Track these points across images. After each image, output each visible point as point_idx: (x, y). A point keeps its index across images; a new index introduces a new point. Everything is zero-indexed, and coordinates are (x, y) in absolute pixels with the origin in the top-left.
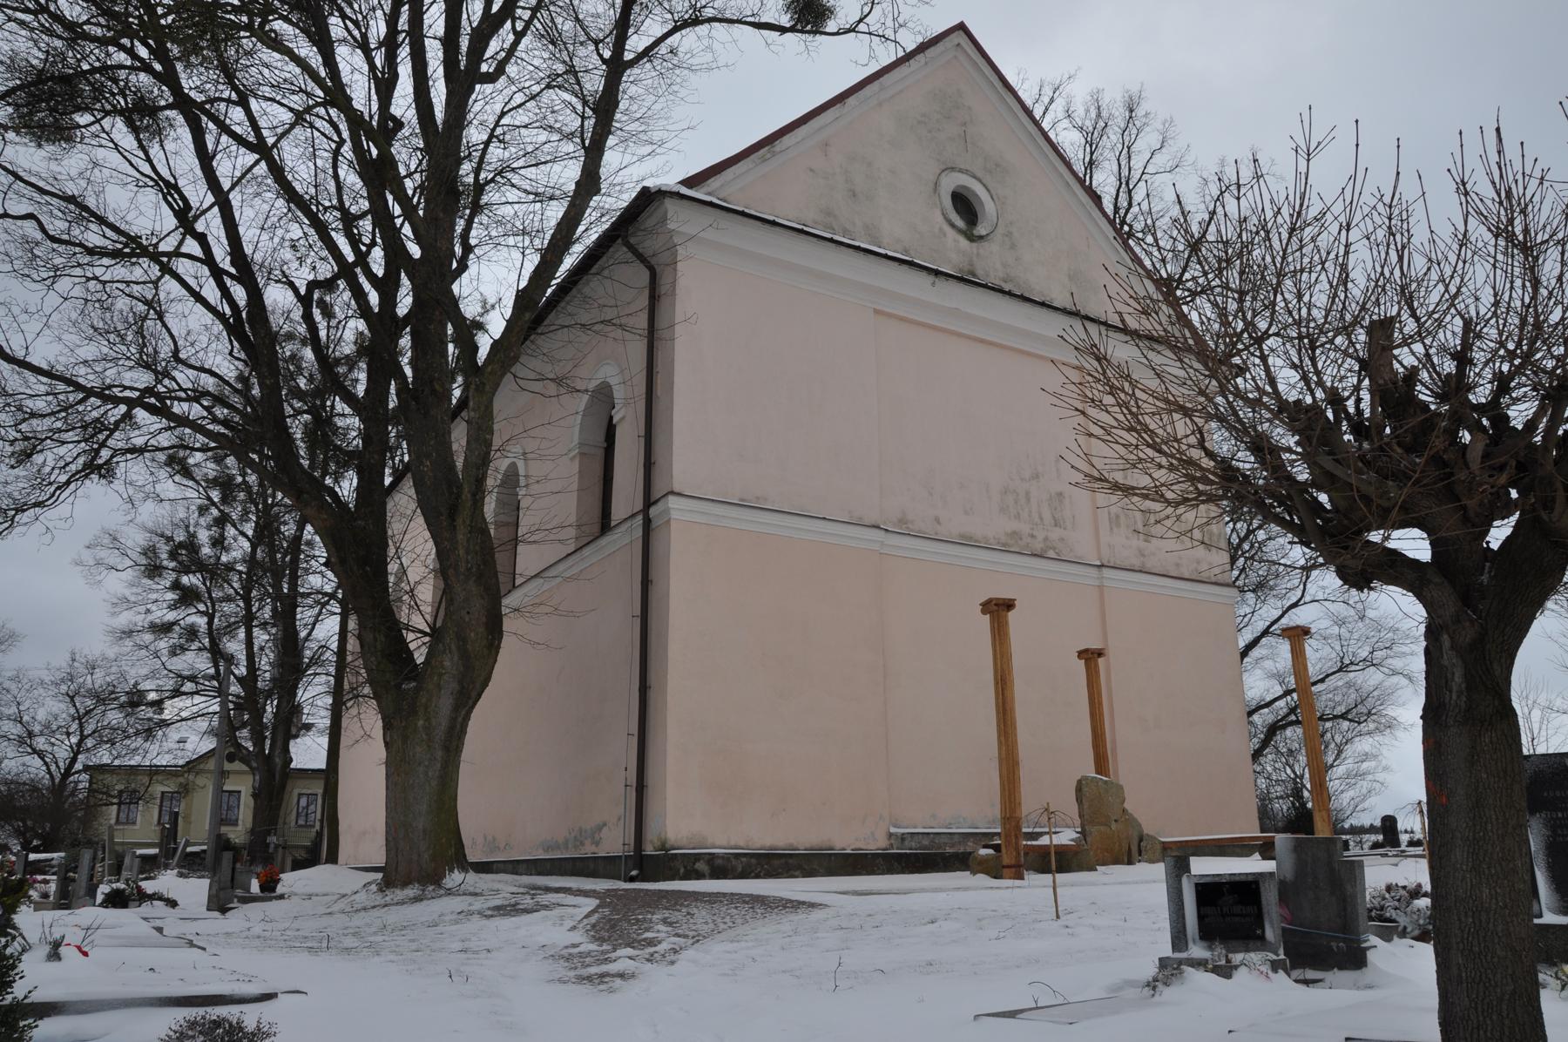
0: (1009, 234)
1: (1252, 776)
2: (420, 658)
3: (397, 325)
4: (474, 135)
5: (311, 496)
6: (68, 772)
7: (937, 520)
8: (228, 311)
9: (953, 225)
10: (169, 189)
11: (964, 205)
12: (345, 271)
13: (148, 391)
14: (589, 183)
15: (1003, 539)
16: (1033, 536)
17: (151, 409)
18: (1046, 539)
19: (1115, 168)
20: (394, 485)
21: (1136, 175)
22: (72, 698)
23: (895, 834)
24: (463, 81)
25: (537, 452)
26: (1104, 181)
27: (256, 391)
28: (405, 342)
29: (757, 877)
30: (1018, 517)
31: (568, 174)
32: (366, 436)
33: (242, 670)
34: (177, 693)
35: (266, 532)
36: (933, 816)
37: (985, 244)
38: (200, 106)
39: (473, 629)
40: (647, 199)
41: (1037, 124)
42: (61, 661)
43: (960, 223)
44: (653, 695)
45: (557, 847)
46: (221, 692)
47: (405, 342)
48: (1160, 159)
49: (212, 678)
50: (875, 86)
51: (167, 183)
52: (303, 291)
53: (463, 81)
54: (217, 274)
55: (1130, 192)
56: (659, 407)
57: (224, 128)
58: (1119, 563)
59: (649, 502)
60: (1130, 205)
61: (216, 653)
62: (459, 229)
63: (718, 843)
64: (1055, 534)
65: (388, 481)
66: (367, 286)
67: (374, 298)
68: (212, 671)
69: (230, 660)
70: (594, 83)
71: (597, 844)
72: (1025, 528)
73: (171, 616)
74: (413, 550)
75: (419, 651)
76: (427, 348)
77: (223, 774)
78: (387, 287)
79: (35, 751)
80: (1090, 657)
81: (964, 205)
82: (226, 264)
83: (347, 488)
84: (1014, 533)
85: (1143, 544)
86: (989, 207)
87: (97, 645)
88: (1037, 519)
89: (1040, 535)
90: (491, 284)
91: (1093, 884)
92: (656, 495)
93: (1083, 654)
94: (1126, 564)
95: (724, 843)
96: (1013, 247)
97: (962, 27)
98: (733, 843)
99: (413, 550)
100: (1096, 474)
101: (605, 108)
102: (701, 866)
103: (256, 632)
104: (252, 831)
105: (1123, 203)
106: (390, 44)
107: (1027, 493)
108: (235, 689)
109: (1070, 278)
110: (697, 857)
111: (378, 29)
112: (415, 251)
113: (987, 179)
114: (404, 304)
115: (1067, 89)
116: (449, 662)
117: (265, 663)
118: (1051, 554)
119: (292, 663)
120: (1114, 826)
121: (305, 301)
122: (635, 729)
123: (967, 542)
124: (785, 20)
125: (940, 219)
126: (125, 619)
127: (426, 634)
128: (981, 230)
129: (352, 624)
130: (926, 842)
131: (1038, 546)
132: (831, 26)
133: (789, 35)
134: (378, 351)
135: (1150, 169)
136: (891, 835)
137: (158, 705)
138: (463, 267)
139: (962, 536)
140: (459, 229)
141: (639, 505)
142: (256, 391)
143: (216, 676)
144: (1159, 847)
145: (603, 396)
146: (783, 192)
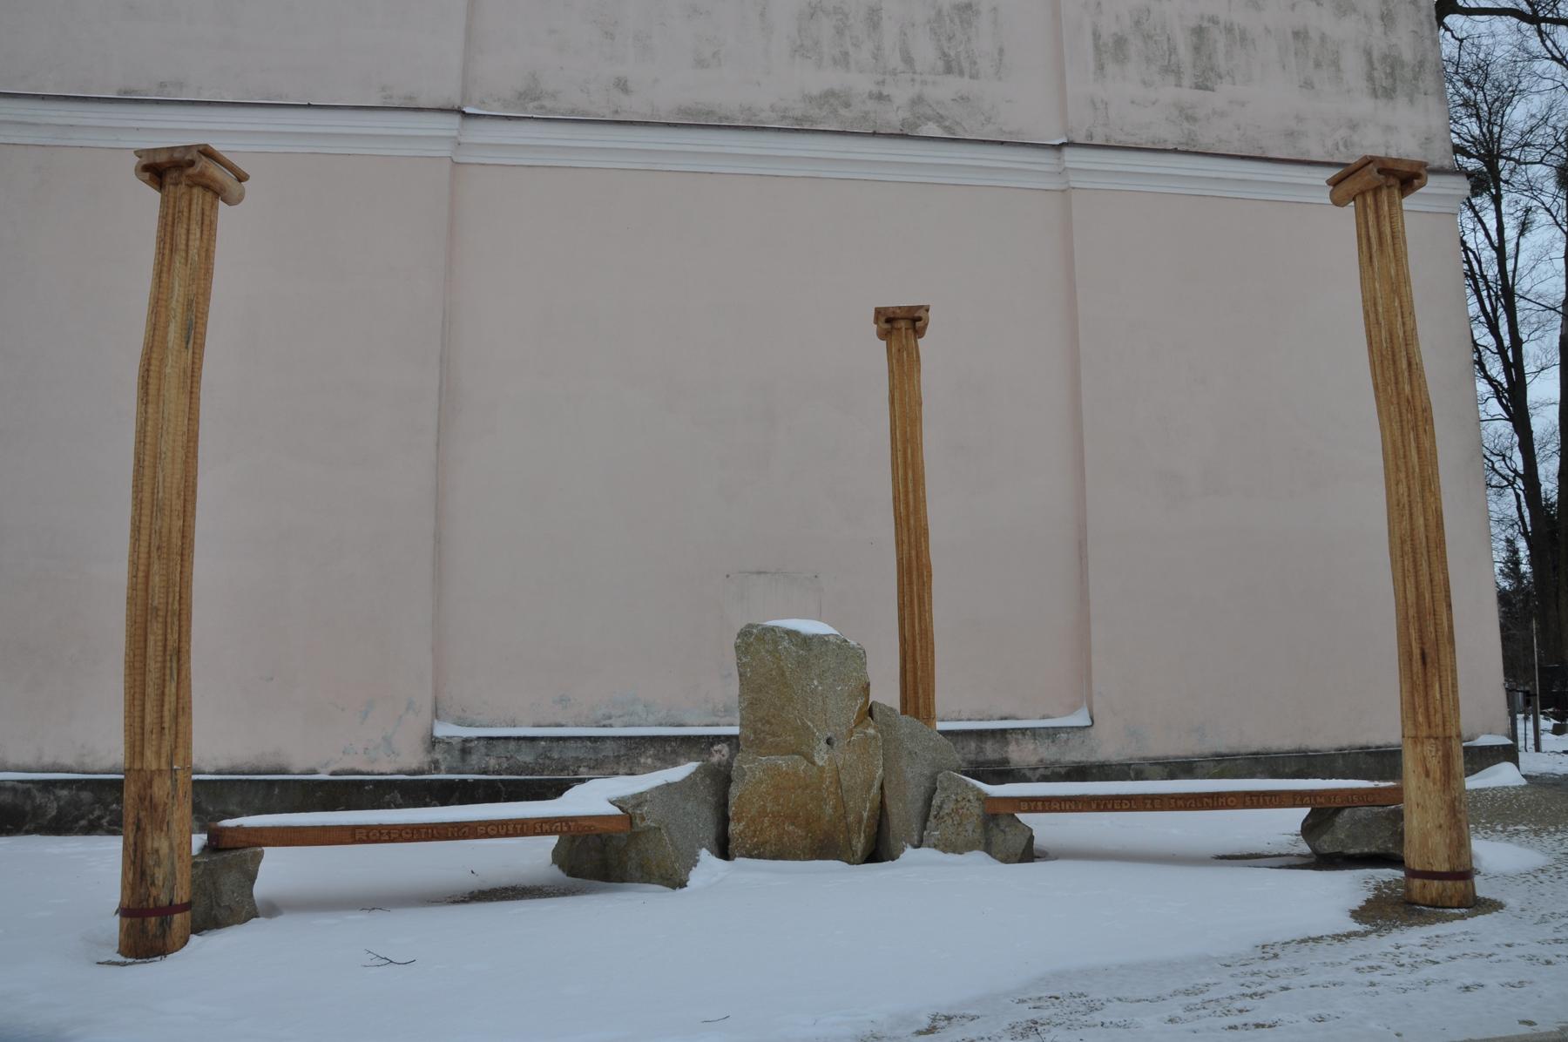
7: (622, 86)
16: (880, 97)
18: (918, 101)
23: (448, 742)
30: (843, 60)
58: (1119, 138)
64: (944, 90)
72: (861, 83)
80: (901, 325)
84: (830, 94)
85: (1188, 95)
88: (895, 61)
89: (901, 94)
93: (161, 170)
95: (28, 758)
98: (47, 760)
100: (1510, 248)
118: (931, 129)
120: (821, 757)
130: (526, 756)
131: (894, 118)
136: (434, 742)
144: (976, 809)
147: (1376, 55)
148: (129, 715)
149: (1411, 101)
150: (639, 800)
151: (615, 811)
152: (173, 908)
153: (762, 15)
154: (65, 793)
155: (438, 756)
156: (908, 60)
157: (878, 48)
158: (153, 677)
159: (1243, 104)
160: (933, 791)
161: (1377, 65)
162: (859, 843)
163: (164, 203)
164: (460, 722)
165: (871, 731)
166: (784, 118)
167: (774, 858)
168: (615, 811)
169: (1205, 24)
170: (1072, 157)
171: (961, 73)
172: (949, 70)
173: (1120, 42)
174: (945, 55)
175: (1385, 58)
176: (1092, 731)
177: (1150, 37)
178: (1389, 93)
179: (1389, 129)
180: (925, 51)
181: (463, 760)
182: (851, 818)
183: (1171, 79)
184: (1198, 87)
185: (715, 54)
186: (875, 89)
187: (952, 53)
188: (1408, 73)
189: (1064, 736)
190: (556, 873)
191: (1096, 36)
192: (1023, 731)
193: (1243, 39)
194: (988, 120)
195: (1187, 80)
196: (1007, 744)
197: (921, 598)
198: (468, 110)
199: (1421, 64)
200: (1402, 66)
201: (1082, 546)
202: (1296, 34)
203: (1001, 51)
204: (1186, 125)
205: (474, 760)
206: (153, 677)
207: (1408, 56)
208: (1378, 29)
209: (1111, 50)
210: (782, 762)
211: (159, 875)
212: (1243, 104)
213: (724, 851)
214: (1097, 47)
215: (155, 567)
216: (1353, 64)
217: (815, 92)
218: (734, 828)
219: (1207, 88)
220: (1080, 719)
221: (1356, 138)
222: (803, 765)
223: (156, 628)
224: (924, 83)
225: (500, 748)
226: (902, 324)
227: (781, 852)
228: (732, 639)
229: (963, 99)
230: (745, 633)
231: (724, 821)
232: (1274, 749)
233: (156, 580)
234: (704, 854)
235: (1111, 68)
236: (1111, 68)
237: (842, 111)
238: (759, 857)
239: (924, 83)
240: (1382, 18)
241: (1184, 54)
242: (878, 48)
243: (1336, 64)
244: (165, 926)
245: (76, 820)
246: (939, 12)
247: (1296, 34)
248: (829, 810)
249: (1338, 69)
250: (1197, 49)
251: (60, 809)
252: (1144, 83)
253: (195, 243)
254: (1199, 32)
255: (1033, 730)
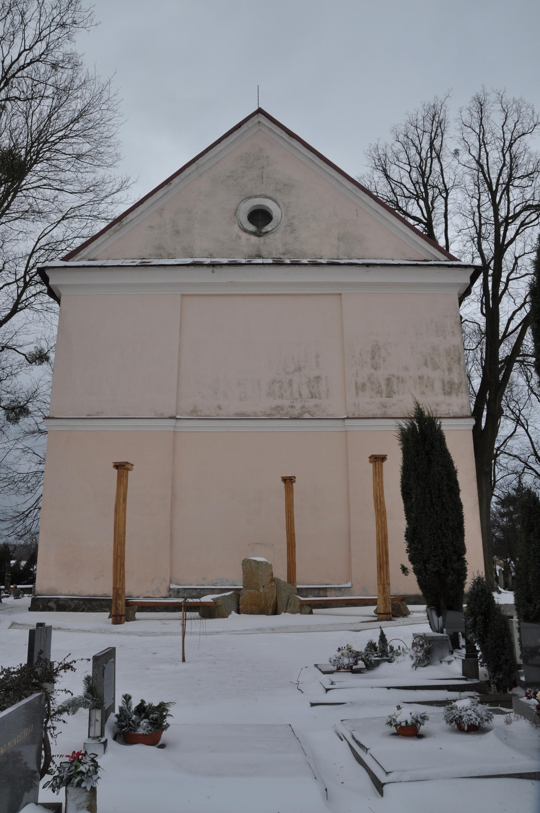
1: (79, 790)
7: (219, 407)
15: (269, 412)
16: (292, 407)
18: (303, 407)
19: (395, 179)
27: (493, 461)
29: (83, 611)
30: (281, 396)
36: (204, 579)
37: (271, 236)
50: (193, 167)
58: (363, 415)
63: (63, 593)
64: (311, 403)
72: (286, 403)
84: (277, 407)
85: (384, 399)
88: (296, 395)
89: (298, 405)
91: (308, 629)
94: (370, 414)
95: (67, 593)
96: (293, 231)
97: (260, 111)
98: (71, 593)
102: (51, 604)
110: (50, 600)
118: (307, 416)
120: (261, 590)
123: (242, 417)
131: (296, 413)
136: (170, 589)
139: (237, 414)
142: (493, 461)
144: (298, 603)
147: (446, 382)
148: (114, 577)
149: (457, 395)
150: (218, 599)
151: (212, 601)
152: (122, 615)
153: (258, 384)
154: (76, 601)
155: (171, 593)
156: (300, 395)
157: (292, 392)
158: (119, 569)
159: (402, 401)
160: (289, 599)
161: (446, 385)
162: (270, 611)
163: (118, 472)
164: (177, 584)
165: (273, 584)
166: (264, 414)
167: (250, 614)
168: (212, 601)
169: (390, 377)
170: (347, 422)
171: (316, 398)
172: (312, 397)
173: (364, 385)
174: (311, 392)
175: (448, 382)
176: (352, 589)
177: (373, 383)
178: (450, 393)
179: (449, 405)
180: (306, 392)
181: (178, 594)
182: (268, 605)
183: (379, 395)
184: (388, 397)
185: (245, 397)
186: (291, 405)
187: (313, 392)
188: (456, 386)
189: (343, 590)
190: (200, 617)
191: (356, 384)
192: (331, 588)
193: (402, 380)
194: (324, 411)
195: (384, 395)
196: (327, 592)
197: (292, 552)
198: (178, 417)
199: (461, 383)
200: (455, 384)
201: (350, 534)
202: (420, 377)
203: (328, 390)
204: (384, 409)
205: (181, 594)
206: (119, 569)
207: (456, 381)
208: (447, 373)
209: (361, 388)
210: (252, 591)
211: (120, 608)
212: (402, 401)
213: (238, 612)
214: (356, 388)
215: (119, 548)
216: (438, 385)
217: (273, 406)
218: (241, 607)
219: (390, 397)
220: (349, 585)
221: (438, 408)
222: (257, 592)
223: (119, 559)
224: (305, 401)
225: (188, 591)
226: (288, 481)
227: (252, 613)
228: (241, 562)
229: (317, 406)
230: (244, 561)
231: (238, 605)
232: (408, 594)
233: (119, 550)
234: (233, 612)
235: (361, 393)
236: (361, 393)
237: (281, 412)
238: (247, 614)
239: (305, 401)
240: (448, 369)
241: (384, 387)
242: (292, 392)
243: (432, 386)
244: (121, 619)
245: (79, 609)
246: (310, 380)
247: (420, 377)
248: (263, 603)
249: (433, 387)
250: (388, 385)
251: (75, 606)
252: (371, 397)
253: (125, 481)
254: (388, 380)
255: (334, 588)
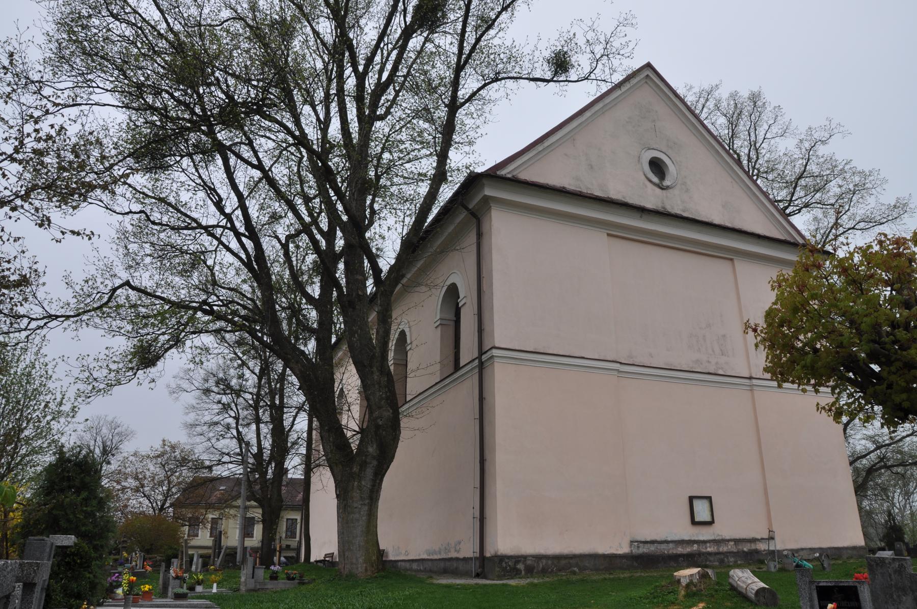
0: (684, 184)
2: (354, 447)
3: (336, 258)
4: (375, 148)
5: (292, 357)
6: (162, 508)
8: (244, 256)
9: (650, 181)
10: (210, 190)
11: (657, 166)
12: (306, 229)
13: (205, 302)
14: (440, 177)
16: (709, 362)
17: (205, 312)
18: (717, 363)
20: (336, 343)
21: (760, 138)
22: (164, 466)
24: (367, 121)
25: (418, 322)
26: (741, 146)
28: (341, 266)
31: (428, 165)
32: (320, 323)
33: (255, 450)
34: (220, 463)
35: (265, 371)
38: (229, 148)
39: (383, 435)
40: (473, 181)
41: (697, 117)
42: (158, 445)
43: (655, 180)
44: (487, 465)
45: (435, 553)
46: (243, 462)
47: (341, 266)
48: (775, 129)
49: (238, 454)
51: (210, 188)
52: (283, 242)
53: (367, 121)
54: (238, 235)
55: (757, 150)
56: (485, 298)
57: (239, 156)
59: (481, 353)
60: (758, 158)
61: (240, 438)
62: (368, 202)
65: (334, 340)
66: (318, 237)
67: (323, 244)
68: (238, 450)
69: (248, 444)
70: (442, 113)
71: (458, 552)
73: (216, 419)
74: (348, 380)
75: (354, 445)
76: (354, 271)
77: (246, 508)
78: (330, 236)
79: (145, 496)
81: (657, 166)
82: (242, 230)
83: (310, 347)
86: (672, 168)
87: (180, 437)
90: (388, 236)
92: (486, 348)
96: (687, 191)
97: (649, 66)
99: (348, 380)
101: (448, 129)
103: (262, 426)
104: (262, 541)
105: (753, 155)
106: (327, 101)
107: (704, 336)
108: (251, 460)
109: (723, 206)
111: (320, 95)
112: (345, 218)
113: (670, 152)
114: (340, 243)
115: (716, 94)
116: (372, 449)
117: (267, 444)
119: (281, 447)
121: (285, 247)
122: (478, 485)
124: (548, 75)
125: (643, 177)
126: (191, 418)
127: (358, 433)
128: (667, 183)
129: (315, 423)
132: (573, 75)
133: (551, 83)
134: (325, 267)
135: (768, 136)
137: (210, 468)
138: (371, 223)
140: (368, 202)
141: (476, 355)
143: (240, 454)
145: (453, 291)
146: (553, 171)
